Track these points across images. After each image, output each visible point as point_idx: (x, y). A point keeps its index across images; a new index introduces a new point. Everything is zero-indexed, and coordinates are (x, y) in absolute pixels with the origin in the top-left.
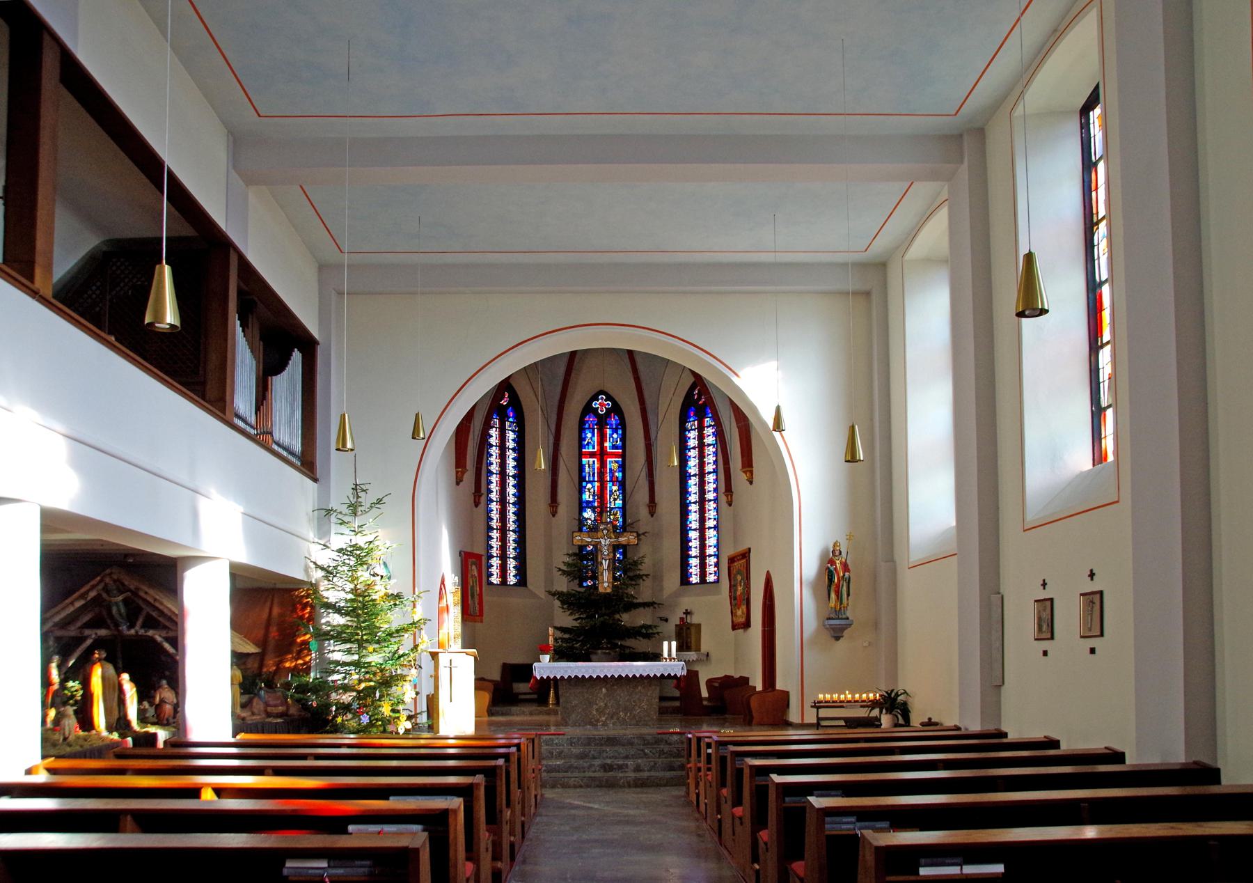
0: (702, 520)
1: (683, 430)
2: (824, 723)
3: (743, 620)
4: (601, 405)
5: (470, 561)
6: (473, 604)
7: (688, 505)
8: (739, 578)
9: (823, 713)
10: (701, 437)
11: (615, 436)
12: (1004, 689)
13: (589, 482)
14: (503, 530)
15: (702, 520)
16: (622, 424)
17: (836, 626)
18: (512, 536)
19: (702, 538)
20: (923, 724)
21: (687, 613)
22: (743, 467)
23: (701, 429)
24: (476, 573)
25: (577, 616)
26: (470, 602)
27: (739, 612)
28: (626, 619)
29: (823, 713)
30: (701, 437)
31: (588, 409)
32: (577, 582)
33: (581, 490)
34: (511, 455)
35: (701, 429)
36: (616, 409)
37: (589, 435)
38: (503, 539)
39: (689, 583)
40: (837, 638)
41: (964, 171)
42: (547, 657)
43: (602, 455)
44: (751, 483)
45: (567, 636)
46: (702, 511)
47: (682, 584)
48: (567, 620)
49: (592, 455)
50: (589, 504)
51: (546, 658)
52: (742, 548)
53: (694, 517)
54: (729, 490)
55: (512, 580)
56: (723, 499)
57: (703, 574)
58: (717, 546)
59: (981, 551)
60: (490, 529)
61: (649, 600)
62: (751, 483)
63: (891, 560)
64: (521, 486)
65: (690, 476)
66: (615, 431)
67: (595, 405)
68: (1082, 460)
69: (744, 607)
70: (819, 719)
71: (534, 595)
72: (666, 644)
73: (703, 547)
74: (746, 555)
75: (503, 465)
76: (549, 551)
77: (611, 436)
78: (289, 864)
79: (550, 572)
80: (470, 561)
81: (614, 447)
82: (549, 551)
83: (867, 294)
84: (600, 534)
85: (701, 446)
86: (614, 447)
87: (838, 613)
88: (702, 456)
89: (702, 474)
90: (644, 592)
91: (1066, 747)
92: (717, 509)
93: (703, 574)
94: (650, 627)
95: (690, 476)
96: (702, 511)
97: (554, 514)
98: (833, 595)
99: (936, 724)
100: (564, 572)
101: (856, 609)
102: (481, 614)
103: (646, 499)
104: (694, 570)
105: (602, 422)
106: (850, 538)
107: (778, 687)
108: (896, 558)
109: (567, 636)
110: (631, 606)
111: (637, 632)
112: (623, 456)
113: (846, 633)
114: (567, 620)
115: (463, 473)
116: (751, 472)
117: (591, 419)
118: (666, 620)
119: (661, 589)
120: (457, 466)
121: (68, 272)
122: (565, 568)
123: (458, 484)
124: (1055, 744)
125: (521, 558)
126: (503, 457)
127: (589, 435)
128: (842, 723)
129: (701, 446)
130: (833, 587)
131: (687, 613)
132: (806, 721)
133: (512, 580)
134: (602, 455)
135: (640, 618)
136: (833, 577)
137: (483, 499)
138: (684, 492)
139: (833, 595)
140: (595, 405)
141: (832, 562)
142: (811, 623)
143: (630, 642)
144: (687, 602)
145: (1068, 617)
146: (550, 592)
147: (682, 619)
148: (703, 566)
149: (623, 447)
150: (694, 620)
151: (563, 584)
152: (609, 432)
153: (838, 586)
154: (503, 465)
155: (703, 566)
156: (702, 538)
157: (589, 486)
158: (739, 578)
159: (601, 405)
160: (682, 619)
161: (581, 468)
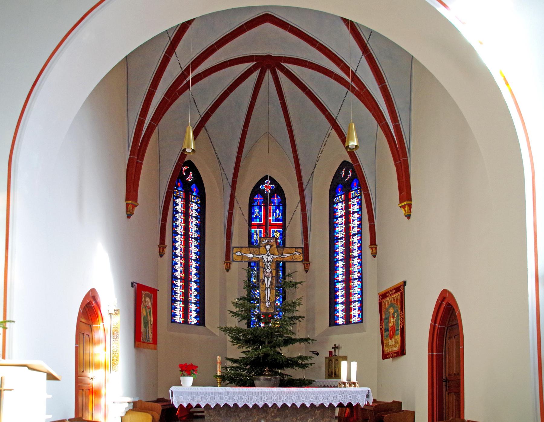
0: (348, 273)
1: (332, 204)
3: (397, 349)
4: (267, 187)
5: (144, 293)
6: (147, 333)
7: (335, 263)
10: (347, 207)
11: (277, 211)
14: (186, 281)
15: (348, 273)
16: (283, 203)
18: (193, 286)
19: (348, 288)
21: (335, 347)
23: (347, 200)
24: (150, 305)
25: (244, 349)
26: (143, 329)
27: (392, 342)
28: (286, 352)
30: (347, 207)
31: (256, 191)
32: (245, 321)
34: (194, 222)
36: (278, 191)
37: (257, 211)
38: (186, 287)
39: (336, 324)
43: (266, 225)
44: (409, 217)
45: (235, 365)
46: (348, 266)
47: (330, 325)
48: (237, 352)
49: (259, 226)
51: (188, 381)
53: (340, 271)
55: (193, 320)
56: (367, 251)
57: (348, 317)
58: (361, 294)
60: (174, 278)
61: (303, 336)
64: (201, 247)
65: (338, 239)
66: (277, 207)
67: (262, 187)
69: (398, 337)
71: (211, 333)
72: (344, 364)
73: (348, 295)
74: (400, 289)
75: (187, 229)
76: (223, 298)
77: (274, 211)
79: (223, 312)
80: (144, 293)
81: (276, 220)
82: (223, 298)
84: (262, 250)
85: (347, 215)
86: (276, 220)
90: (300, 331)
92: (361, 264)
93: (348, 317)
94: (306, 358)
95: (338, 239)
96: (348, 266)
100: (236, 314)
102: (155, 341)
104: (341, 314)
109: (235, 365)
110: (288, 342)
111: (292, 363)
112: (284, 226)
114: (237, 352)
115: (134, 206)
116: (410, 206)
117: (259, 198)
118: (317, 354)
119: (314, 329)
120: (127, 199)
122: (235, 310)
123: (129, 216)
125: (201, 303)
126: (187, 222)
127: (257, 211)
129: (347, 215)
131: (335, 347)
133: (193, 320)
134: (266, 225)
137: (168, 251)
138: (333, 252)
140: (262, 187)
143: (288, 371)
144: (336, 338)
146: (221, 328)
147: (331, 353)
148: (348, 310)
149: (284, 220)
151: (234, 323)
152: (272, 208)
154: (187, 229)
155: (348, 310)
156: (348, 288)
158: (391, 310)
159: (267, 187)
160: (331, 353)
161: (250, 236)
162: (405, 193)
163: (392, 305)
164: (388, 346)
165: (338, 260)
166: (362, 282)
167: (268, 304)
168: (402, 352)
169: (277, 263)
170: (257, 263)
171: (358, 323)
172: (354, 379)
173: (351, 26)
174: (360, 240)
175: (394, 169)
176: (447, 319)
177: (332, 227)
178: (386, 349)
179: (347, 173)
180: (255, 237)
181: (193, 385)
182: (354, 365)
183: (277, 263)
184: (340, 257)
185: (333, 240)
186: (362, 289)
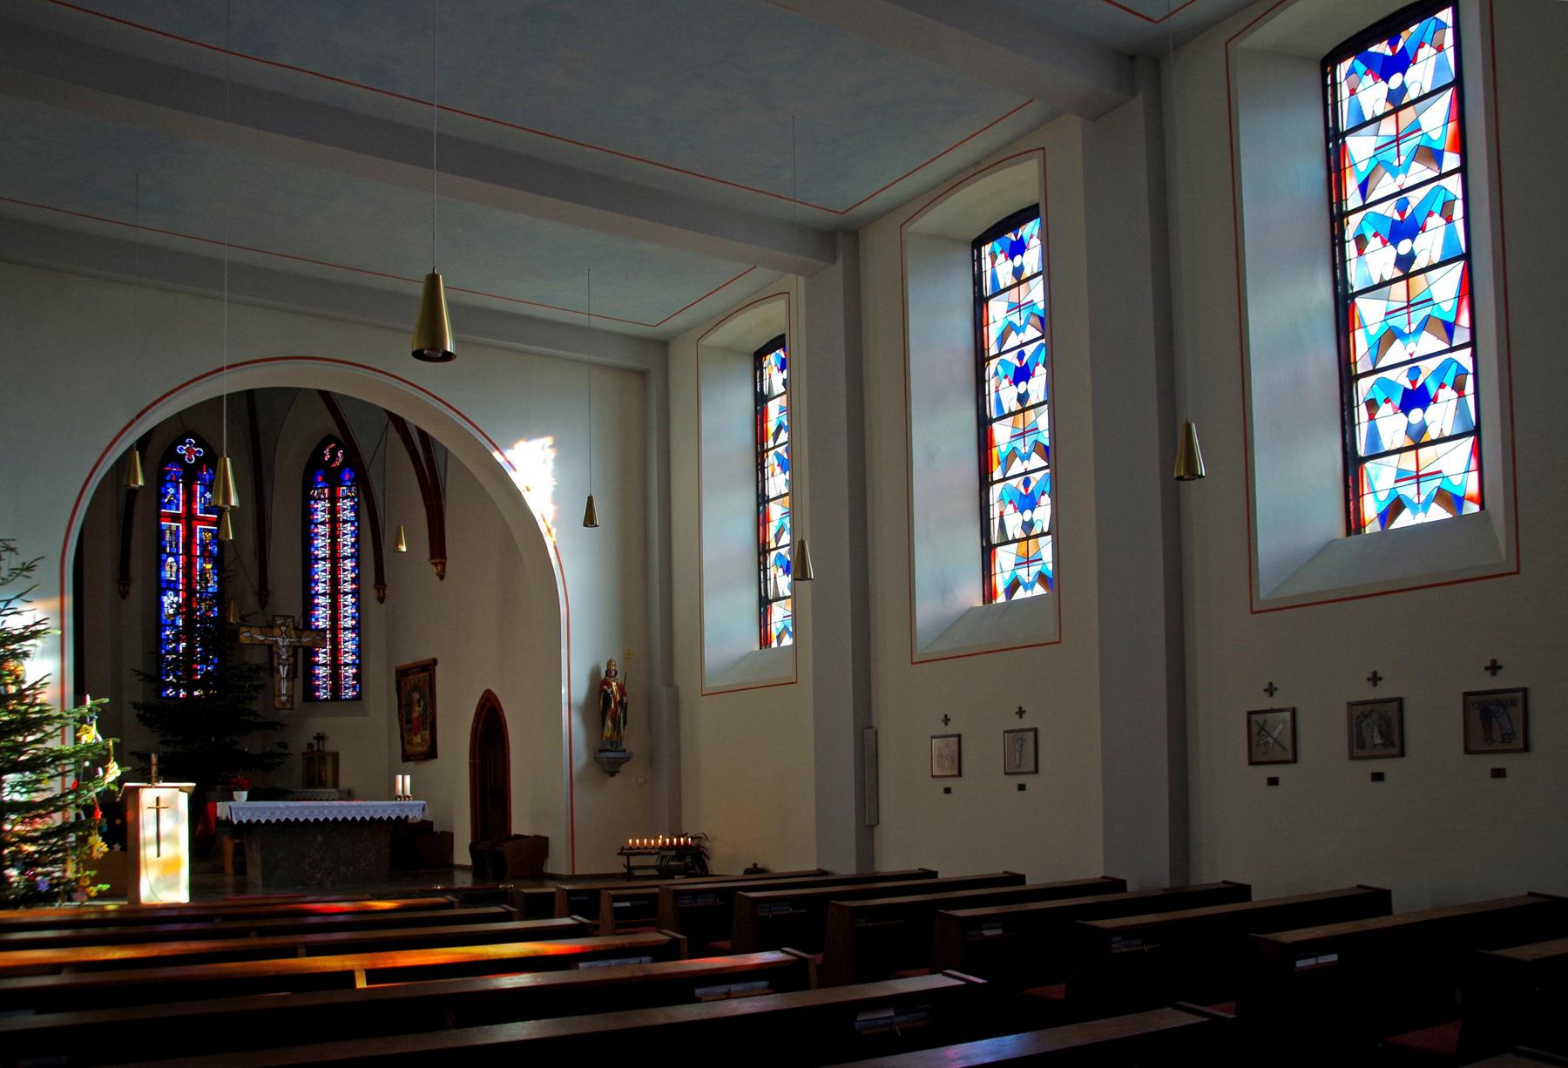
1: (307, 499)
2: (637, 873)
8: (416, 696)
9: (634, 861)
10: (333, 511)
12: (877, 831)
13: (170, 555)
17: (609, 757)
20: (747, 872)
22: (433, 556)
23: (333, 499)
27: (417, 739)
29: (634, 861)
30: (333, 511)
33: (160, 565)
35: (333, 499)
37: (171, 491)
40: (612, 774)
41: (838, 268)
42: (245, 794)
43: (189, 519)
44: (442, 578)
49: (175, 518)
50: (172, 586)
52: (423, 655)
54: (380, 582)
56: (371, 593)
57: (336, 688)
58: (359, 652)
59: (855, 681)
62: (442, 578)
63: (671, 684)
65: (317, 559)
67: (182, 450)
68: (971, 595)
69: (427, 734)
70: (628, 866)
74: (429, 667)
77: (202, 495)
78: (860, 1018)
81: (205, 510)
83: (643, 375)
84: (276, 631)
85: (334, 522)
86: (205, 510)
87: (615, 744)
88: (334, 535)
89: (335, 558)
91: (1032, 881)
92: (357, 605)
93: (336, 688)
97: (124, 595)
98: (609, 723)
99: (762, 871)
101: (632, 741)
103: (256, 582)
105: (334, 481)
106: (627, 657)
107: (514, 832)
108: (678, 681)
113: (622, 768)
116: (444, 565)
121: (1498, 422)
124: (1020, 879)
127: (171, 491)
128: (654, 872)
129: (334, 522)
130: (609, 714)
131: (320, 738)
132: (578, 872)
135: (252, 745)
136: (604, 703)
138: (308, 580)
139: (609, 723)
140: (182, 450)
141: (606, 683)
142: (581, 756)
144: (320, 723)
145: (986, 753)
147: (310, 746)
150: (329, 746)
153: (615, 712)
157: (171, 559)
158: (416, 696)
160: (310, 746)
161: (160, 534)
162: (438, 550)
163: (415, 688)
164: (410, 743)
165: (317, 594)
166: (359, 635)
167: (284, 698)
168: (432, 753)
169: (295, 649)
170: (270, 647)
171: (353, 698)
172: (408, 792)
173: (399, 423)
174: (357, 567)
175: (424, 511)
176: (490, 728)
177: (308, 539)
178: (408, 748)
179: (334, 453)
180: (168, 537)
181: (249, 799)
182: (408, 778)
183: (295, 649)
184: (320, 588)
185: (308, 560)
186: (359, 646)
